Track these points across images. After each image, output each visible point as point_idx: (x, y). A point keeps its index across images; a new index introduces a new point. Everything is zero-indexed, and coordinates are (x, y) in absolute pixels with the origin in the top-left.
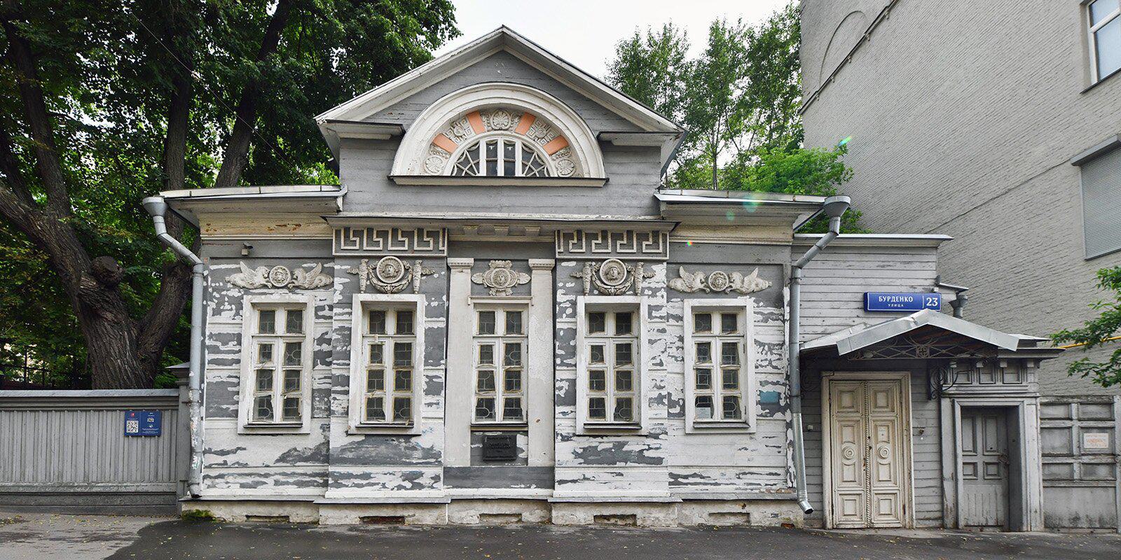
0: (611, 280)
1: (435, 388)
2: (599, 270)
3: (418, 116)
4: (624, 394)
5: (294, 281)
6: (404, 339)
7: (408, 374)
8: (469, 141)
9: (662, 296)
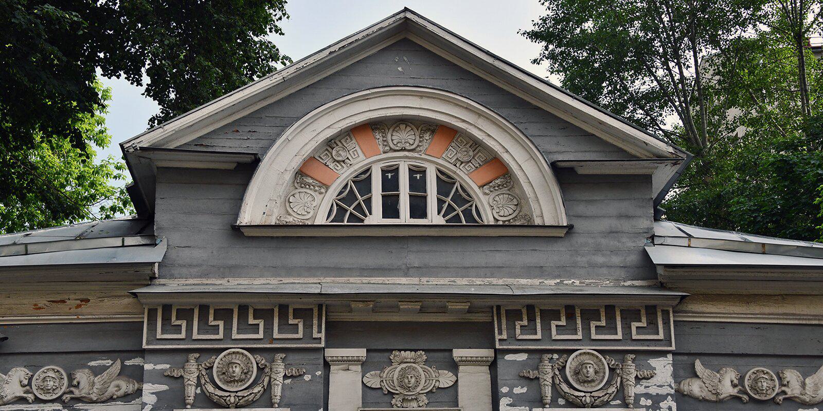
0: (585, 382)
2: (564, 367)
3: (279, 135)
8: (356, 167)
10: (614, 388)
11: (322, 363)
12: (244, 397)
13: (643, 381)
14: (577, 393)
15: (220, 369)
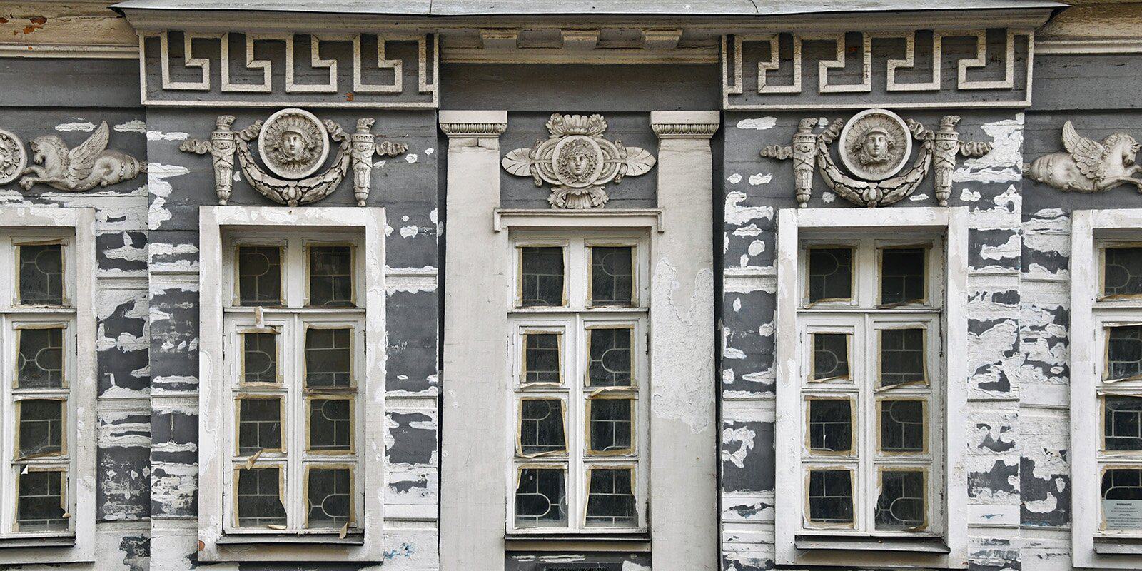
0: (869, 164)
1: (415, 444)
2: (837, 140)
4: (903, 462)
5: (35, 168)
6: (331, 320)
7: (342, 409)
9: (1011, 206)
10: (919, 173)
11: (436, 134)
12: (310, 188)
13: (970, 160)
14: (855, 184)
15: (270, 143)
